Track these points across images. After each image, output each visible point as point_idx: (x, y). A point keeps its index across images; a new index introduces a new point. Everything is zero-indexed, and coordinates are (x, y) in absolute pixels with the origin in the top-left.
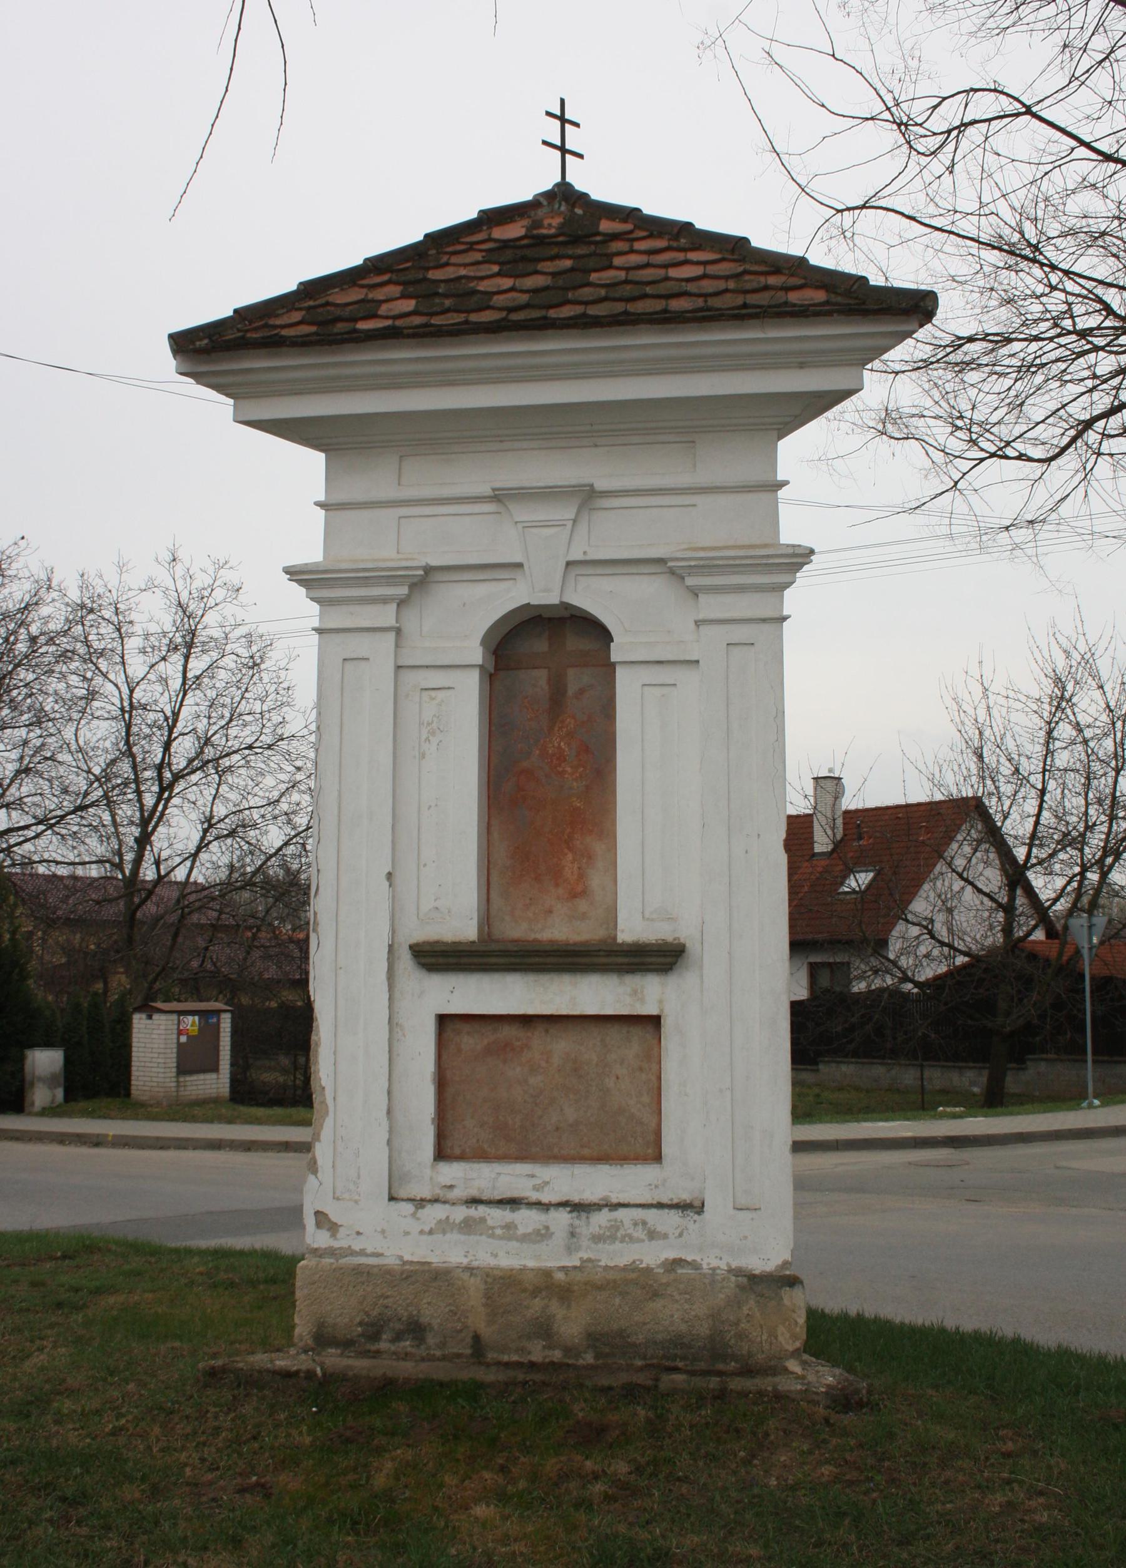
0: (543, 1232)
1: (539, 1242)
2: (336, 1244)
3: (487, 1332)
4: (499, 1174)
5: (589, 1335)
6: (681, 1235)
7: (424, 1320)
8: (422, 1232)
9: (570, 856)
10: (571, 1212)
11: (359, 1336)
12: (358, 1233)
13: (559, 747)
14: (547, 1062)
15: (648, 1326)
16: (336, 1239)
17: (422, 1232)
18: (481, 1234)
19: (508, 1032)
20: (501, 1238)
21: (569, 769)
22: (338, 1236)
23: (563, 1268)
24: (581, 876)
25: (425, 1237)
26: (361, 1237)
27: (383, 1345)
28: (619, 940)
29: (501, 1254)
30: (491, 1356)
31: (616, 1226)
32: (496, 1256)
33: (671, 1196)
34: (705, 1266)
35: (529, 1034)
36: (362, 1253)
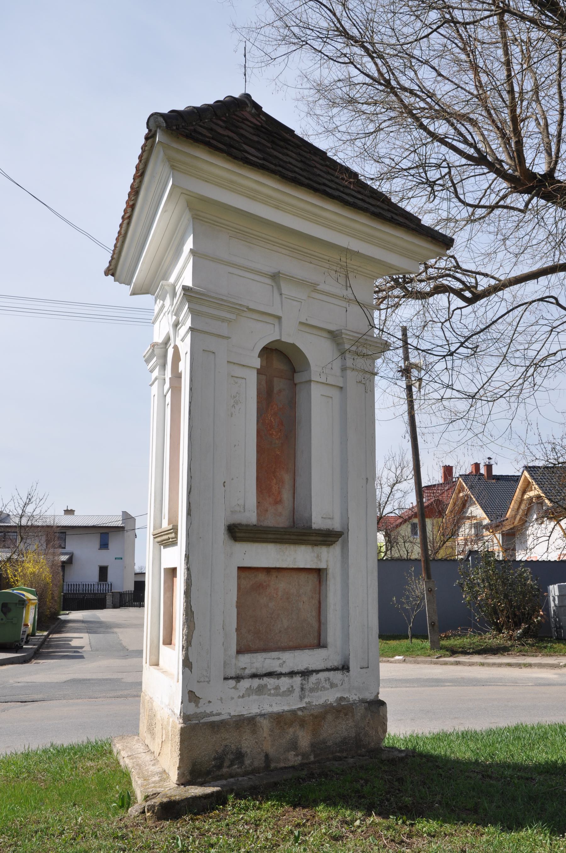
0: (291, 689)
1: (289, 695)
2: (198, 711)
3: (271, 751)
4: (265, 659)
5: (312, 745)
6: (342, 684)
7: (244, 750)
8: (239, 697)
9: (275, 481)
10: (301, 676)
11: (213, 767)
12: (210, 702)
13: (271, 420)
14: (277, 594)
15: (334, 735)
16: (198, 707)
17: (239, 697)
18: (265, 694)
19: (262, 577)
20: (274, 695)
21: (274, 433)
22: (200, 705)
23: (300, 709)
24: (279, 493)
25: (240, 700)
26: (211, 704)
27: (225, 770)
28: (313, 528)
29: (274, 705)
30: (273, 765)
31: (318, 682)
32: (271, 706)
33: (331, 664)
34: (351, 700)
35: (270, 579)
36: (211, 714)
